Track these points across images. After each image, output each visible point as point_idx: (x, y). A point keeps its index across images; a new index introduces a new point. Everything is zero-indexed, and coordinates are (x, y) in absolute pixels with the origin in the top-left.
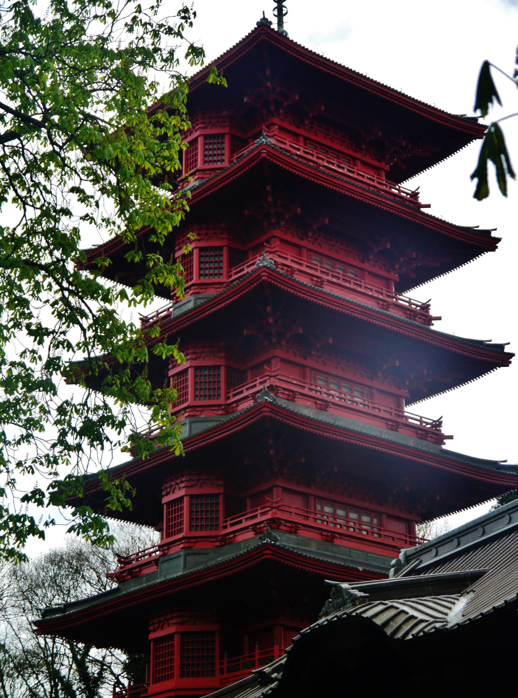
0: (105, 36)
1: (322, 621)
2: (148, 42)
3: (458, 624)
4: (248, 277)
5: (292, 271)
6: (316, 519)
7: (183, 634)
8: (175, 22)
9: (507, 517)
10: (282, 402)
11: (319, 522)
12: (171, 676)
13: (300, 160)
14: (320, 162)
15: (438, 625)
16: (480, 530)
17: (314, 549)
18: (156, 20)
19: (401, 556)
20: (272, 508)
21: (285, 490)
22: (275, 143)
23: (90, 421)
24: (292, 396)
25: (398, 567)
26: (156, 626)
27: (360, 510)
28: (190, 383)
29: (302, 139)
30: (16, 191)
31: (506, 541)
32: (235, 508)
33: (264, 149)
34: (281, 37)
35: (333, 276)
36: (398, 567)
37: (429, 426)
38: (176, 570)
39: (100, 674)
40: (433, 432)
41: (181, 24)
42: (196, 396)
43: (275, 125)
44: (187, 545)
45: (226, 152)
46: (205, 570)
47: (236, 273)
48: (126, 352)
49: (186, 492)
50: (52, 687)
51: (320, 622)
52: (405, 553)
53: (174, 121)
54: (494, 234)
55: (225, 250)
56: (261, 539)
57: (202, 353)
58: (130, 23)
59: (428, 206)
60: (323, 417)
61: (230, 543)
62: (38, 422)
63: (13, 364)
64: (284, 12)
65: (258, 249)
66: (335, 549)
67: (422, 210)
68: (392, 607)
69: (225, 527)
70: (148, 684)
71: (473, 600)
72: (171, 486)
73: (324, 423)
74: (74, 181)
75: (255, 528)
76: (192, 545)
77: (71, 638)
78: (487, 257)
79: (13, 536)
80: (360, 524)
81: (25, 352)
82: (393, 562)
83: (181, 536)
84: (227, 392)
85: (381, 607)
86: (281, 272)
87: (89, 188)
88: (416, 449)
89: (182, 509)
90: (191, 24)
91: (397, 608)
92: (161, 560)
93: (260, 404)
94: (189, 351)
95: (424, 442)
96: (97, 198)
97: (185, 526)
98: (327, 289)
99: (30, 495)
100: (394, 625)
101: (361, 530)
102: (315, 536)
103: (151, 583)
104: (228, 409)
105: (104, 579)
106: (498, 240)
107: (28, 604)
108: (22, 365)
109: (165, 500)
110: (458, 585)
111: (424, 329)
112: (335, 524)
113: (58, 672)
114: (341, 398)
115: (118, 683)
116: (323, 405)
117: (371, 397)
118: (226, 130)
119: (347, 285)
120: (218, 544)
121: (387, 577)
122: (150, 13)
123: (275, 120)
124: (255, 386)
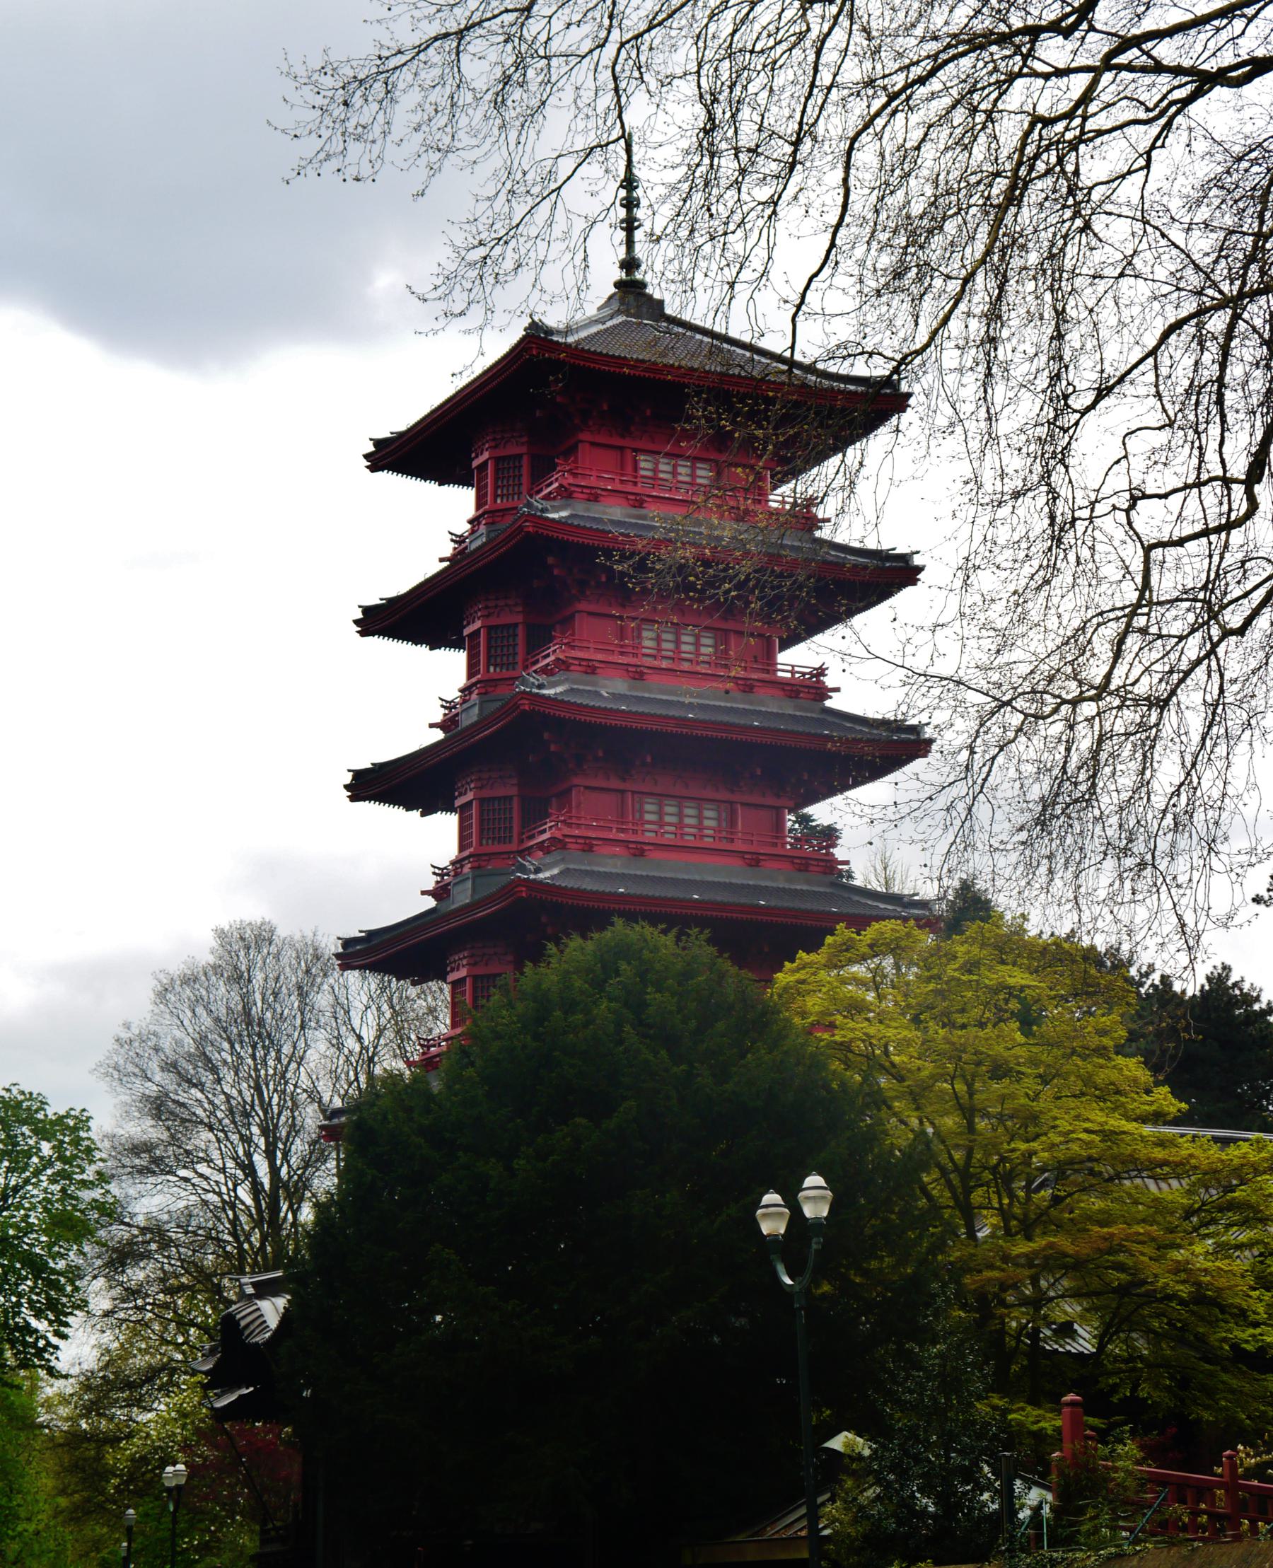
100: (252, 1327)
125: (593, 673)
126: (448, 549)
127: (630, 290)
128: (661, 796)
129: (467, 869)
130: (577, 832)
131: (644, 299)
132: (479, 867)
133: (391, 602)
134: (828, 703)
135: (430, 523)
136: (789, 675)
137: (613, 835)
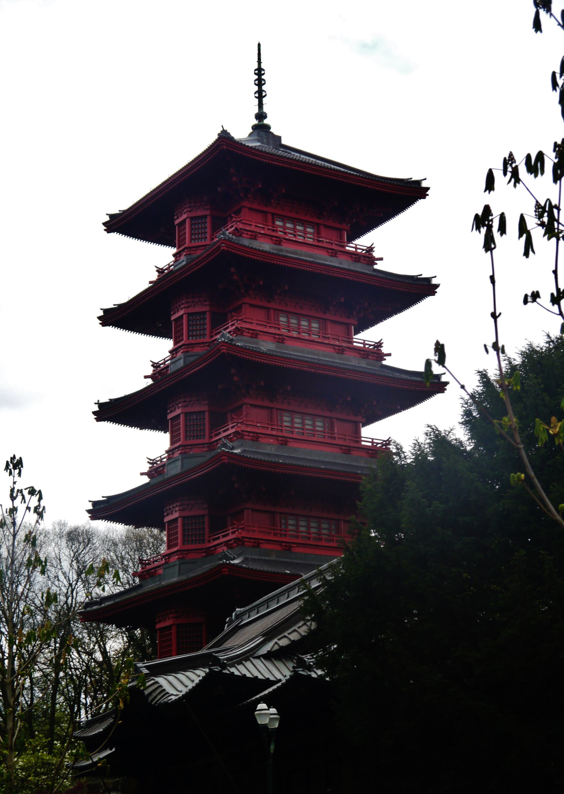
26: (161, 618)
28: (182, 426)
33: (222, 243)
37: (379, 445)
49: (179, 514)
57: (191, 401)
64: (264, 94)
69: (209, 541)
72: (170, 509)
76: (185, 556)
84: (210, 433)
94: (181, 401)
97: (179, 541)
100: (154, 695)
106: (437, 286)
116: (284, 442)
120: (204, 554)
125: (256, 337)
126: (154, 276)
127: (261, 128)
128: (292, 412)
129: (177, 454)
130: (249, 429)
131: (271, 135)
132: (185, 453)
133: (121, 306)
134: (384, 362)
135: (144, 263)
136: (362, 345)
137: (269, 432)
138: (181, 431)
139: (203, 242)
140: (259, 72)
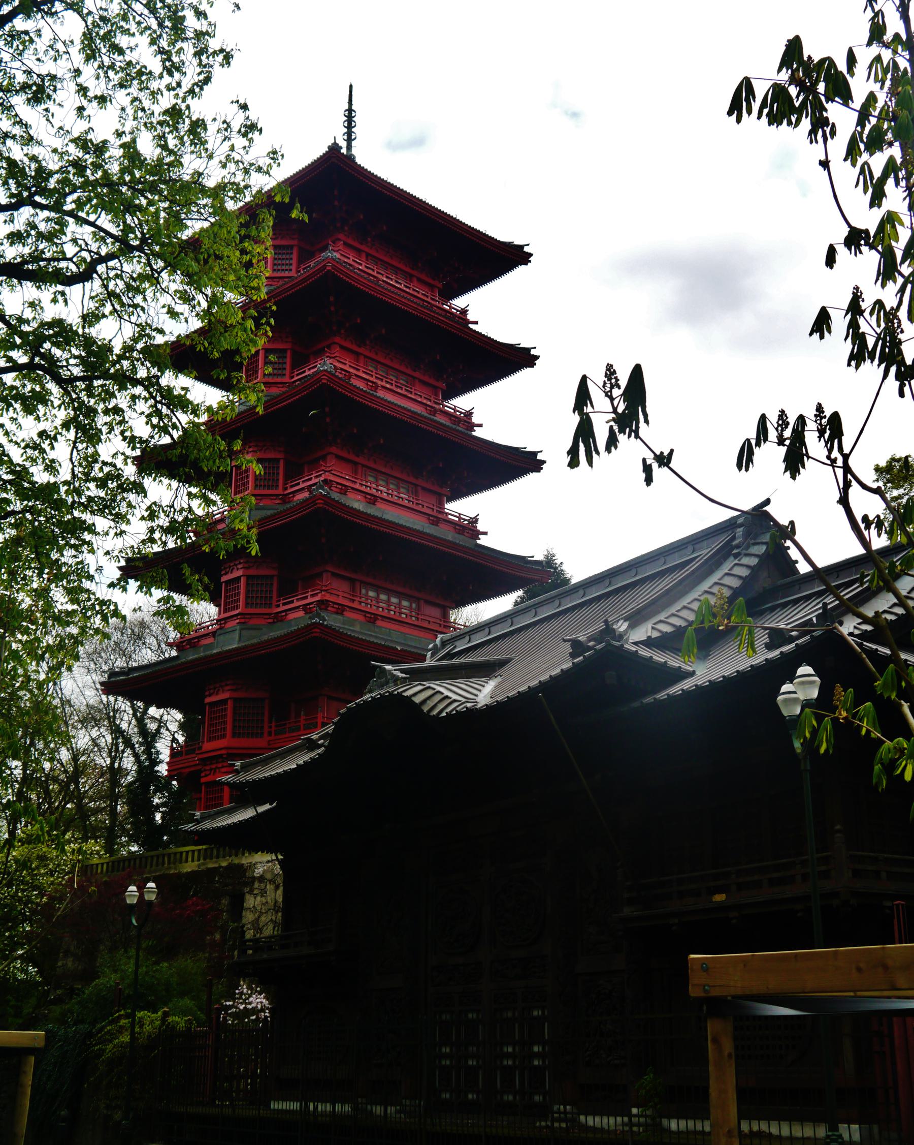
0: (201, 170)
1: (367, 697)
2: (239, 178)
3: (486, 705)
4: (309, 380)
5: (350, 375)
6: (360, 602)
7: (235, 700)
8: (264, 162)
9: (533, 611)
10: (335, 496)
11: (363, 604)
12: (224, 736)
13: (363, 274)
14: (380, 276)
15: (469, 705)
16: (509, 621)
17: (357, 628)
18: (248, 159)
19: (438, 641)
20: (322, 591)
21: (335, 575)
22: (340, 257)
23: (176, 521)
24: (344, 490)
25: (435, 651)
27: (400, 595)
29: (364, 254)
30: (113, 305)
31: (530, 632)
32: (288, 589)
34: (350, 159)
35: (387, 382)
36: (435, 651)
38: (232, 642)
39: (158, 731)
40: (470, 528)
41: (270, 164)
42: (256, 485)
43: (340, 240)
44: (243, 621)
45: (294, 262)
46: (259, 644)
47: (298, 375)
48: (211, 462)
50: (113, 739)
51: (365, 698)
52: (442, 639)
53: (259, 249)
54: (533, 352)
55: (289, 353)
56: (310, 618)
58: (224, 160)
59: (476, 323)
60: (371, 510)
61: (282, 621)
62: (125, 516)
63: (105, 463)
65: (319, 354)
66: (377, 630)
67: (470, 326)
68: (429, 688)
69: (278, 606)
70: (203, 742)
71: (500, 683)
72: (230, 567)
73: (373, 517)
74: (166, 299)
75: (305, 608)
77: (131, 696)
78: (526, 373)
79: (99, 616)
80: (401, 608)
81: (116, 454)
82: (431, 646)
83: (237, 612)
85: (420, 688)
86: (340, 376)
87: (180, 308)
88: (454, 543)
89: (239, 587)
90: (279, 165)
91: (434, 689)
92: (218, 632)
93: (315, 496)
95: (461, 537)
96: (186, 315)
98: (381, 394)
99: (115, 581)
100: (430, 704)
101: (401, 613)
102: (360, 617)
103: (208, 653)
104: (285, 499)
105: (163, 646)
106: (537, 357)
107: (92, 665)
108: (115, 466)
109: (224, 579)
110: (486, 670)
111: (466, 434)
112: (378, 607)
113: (118, 727)
114: (388, 494)
115: (174, 740)
117: (416, 494)
118: (295, 242)
119: (399, 391)
120: (271, 621)
121: (423, 658)
122: (242, 152)
123: (341, 236)
124: (311, 479)
138: (242, 584)
139: (287, 274)
140: (350, 115)
